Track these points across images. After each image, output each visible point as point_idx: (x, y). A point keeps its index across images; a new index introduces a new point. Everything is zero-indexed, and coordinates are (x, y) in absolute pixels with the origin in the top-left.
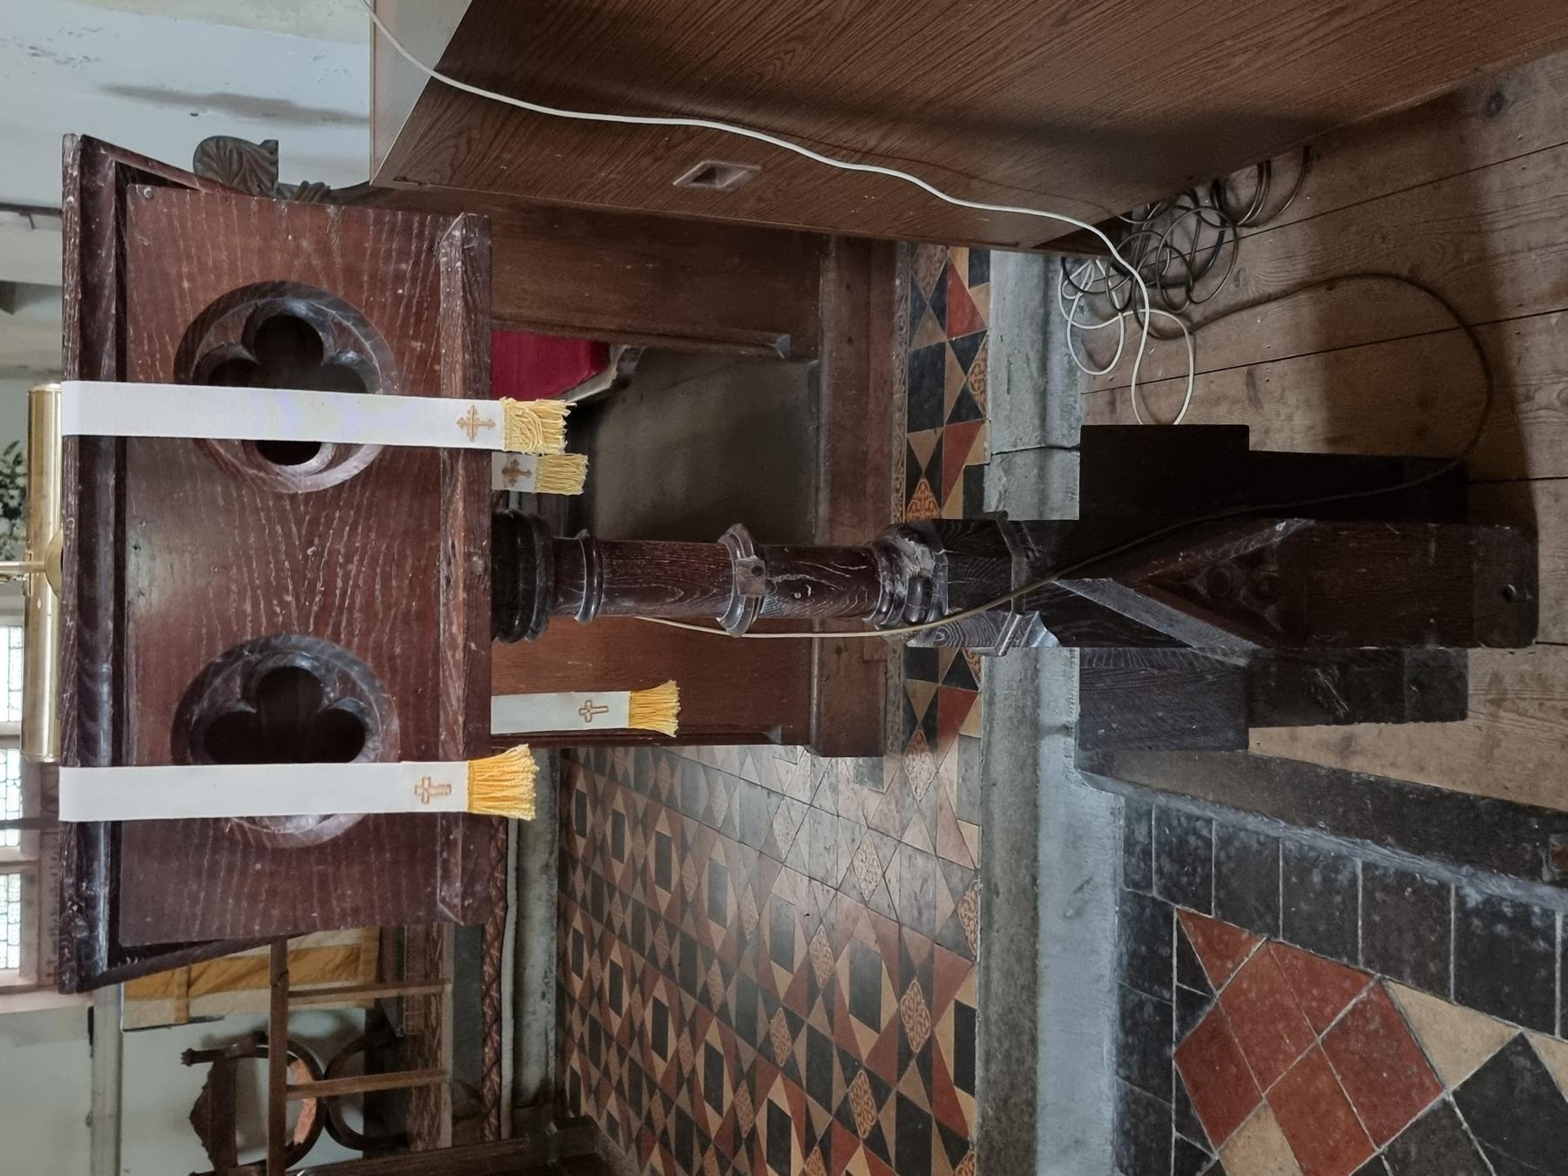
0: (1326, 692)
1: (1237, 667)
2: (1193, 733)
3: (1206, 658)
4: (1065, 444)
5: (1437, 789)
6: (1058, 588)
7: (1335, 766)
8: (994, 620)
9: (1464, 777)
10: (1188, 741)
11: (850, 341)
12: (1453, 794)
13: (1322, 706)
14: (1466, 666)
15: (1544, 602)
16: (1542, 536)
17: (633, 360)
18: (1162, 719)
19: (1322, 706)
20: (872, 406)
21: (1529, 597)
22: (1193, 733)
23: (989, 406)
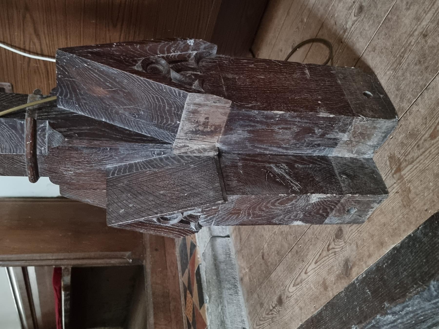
0: (282, 177)
1: (209, 158)
2: (186, 198)
3: (188, 157)
4: (222, 235)
5: (394, 249)
6: (64, 111)
7: (346, 285)
8: (14, 127)
9: (403, 227)
10: (182, 203)
11: (156, 250)
12: (403, 243)
13: (281, 184)
14: (375, 167)
15: (392, 97)
16: (377, 72)
17: (68, 275)
18: (164, 195)
19: (281, 184)
20: (169, 273)
21: (382, 96)
22: (186, 198)
23: (197, 241)
